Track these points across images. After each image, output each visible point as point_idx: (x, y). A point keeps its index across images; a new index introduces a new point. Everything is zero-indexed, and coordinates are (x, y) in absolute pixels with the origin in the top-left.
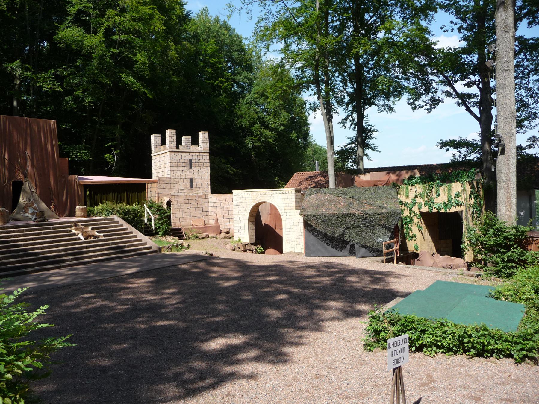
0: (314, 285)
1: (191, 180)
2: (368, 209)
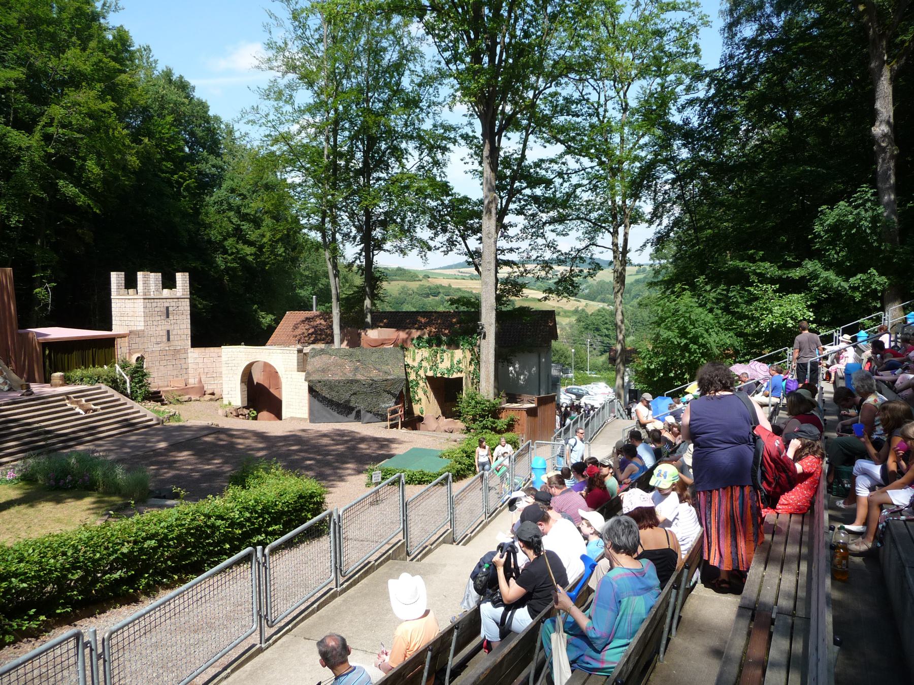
1: (168, 332)
2: (374, 374)
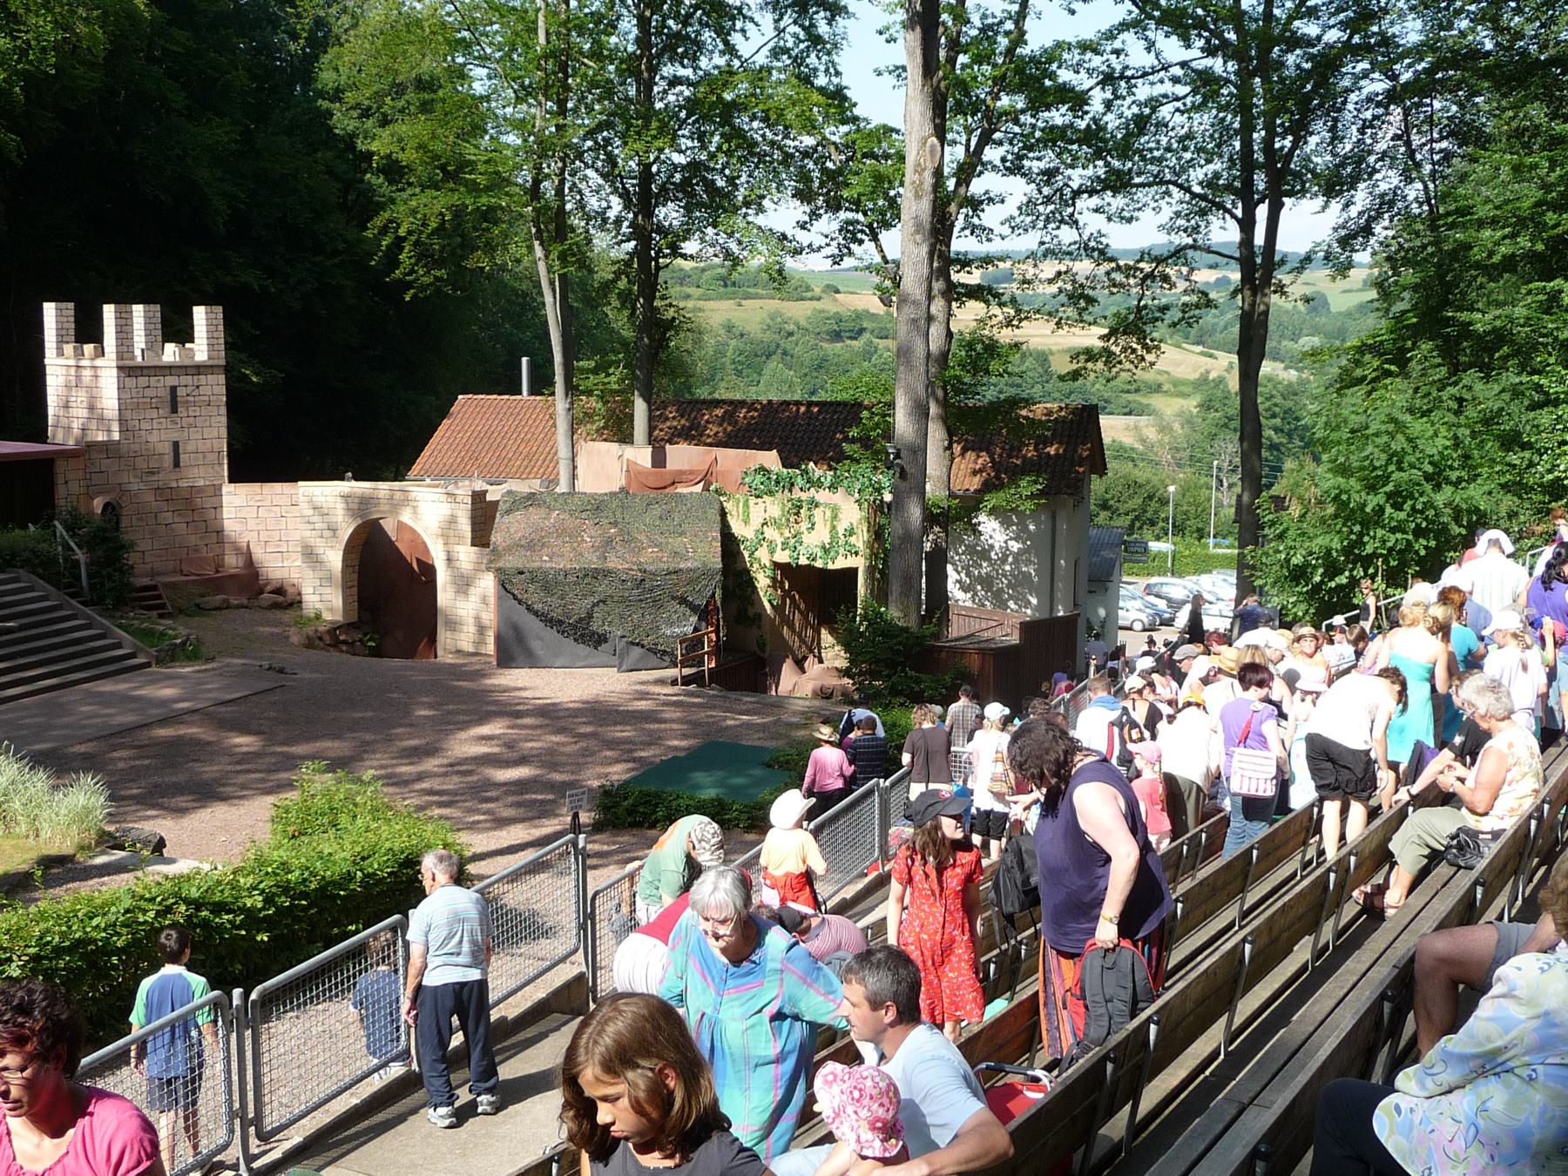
1: (176, 445)
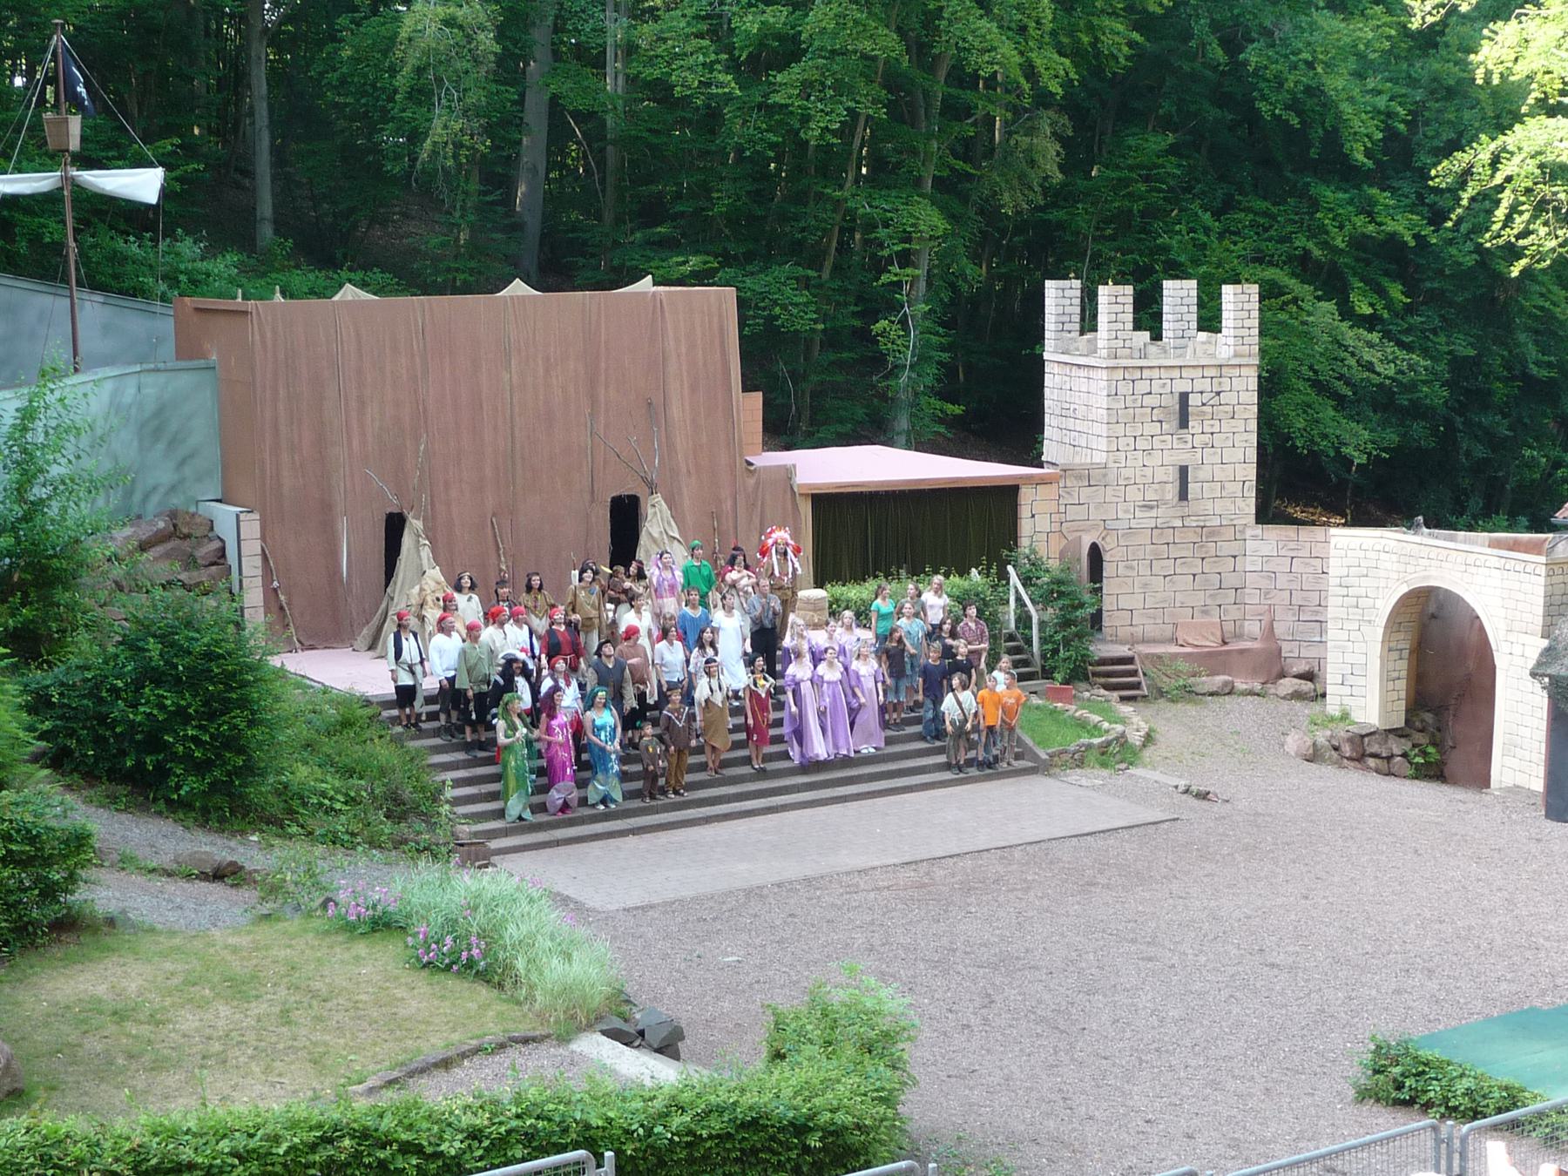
0: (438, 741)
1: (1183, 471)
